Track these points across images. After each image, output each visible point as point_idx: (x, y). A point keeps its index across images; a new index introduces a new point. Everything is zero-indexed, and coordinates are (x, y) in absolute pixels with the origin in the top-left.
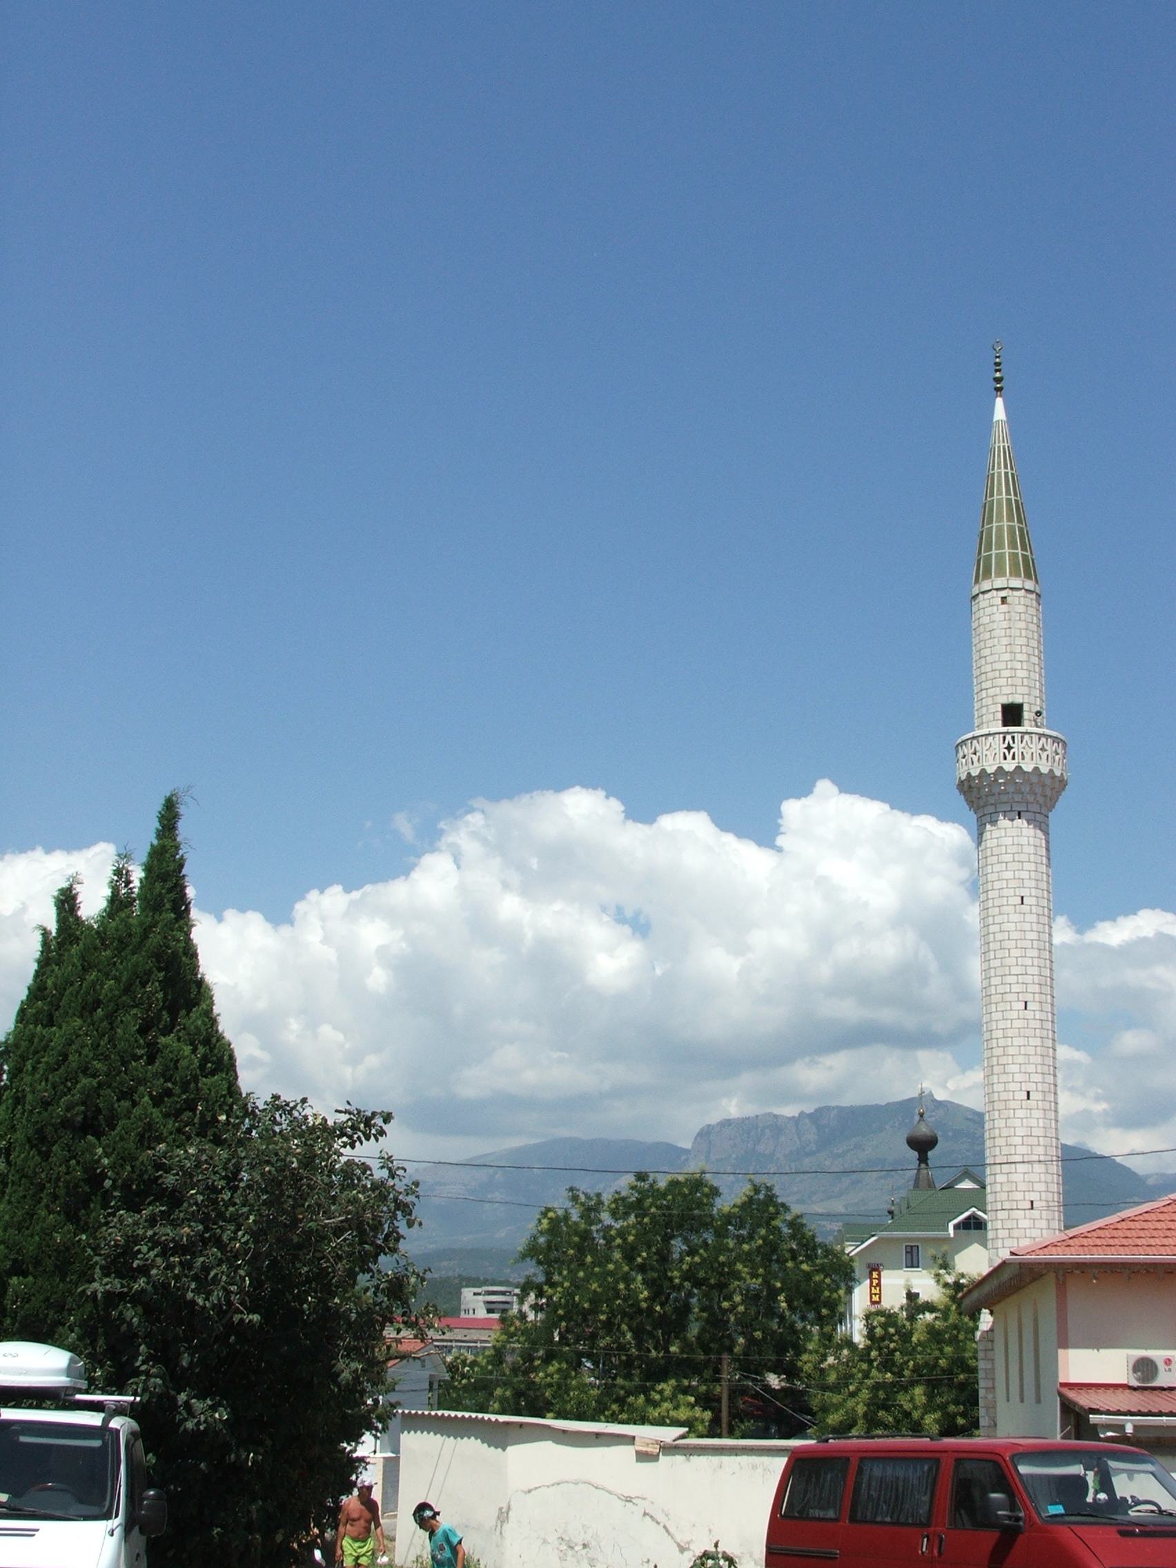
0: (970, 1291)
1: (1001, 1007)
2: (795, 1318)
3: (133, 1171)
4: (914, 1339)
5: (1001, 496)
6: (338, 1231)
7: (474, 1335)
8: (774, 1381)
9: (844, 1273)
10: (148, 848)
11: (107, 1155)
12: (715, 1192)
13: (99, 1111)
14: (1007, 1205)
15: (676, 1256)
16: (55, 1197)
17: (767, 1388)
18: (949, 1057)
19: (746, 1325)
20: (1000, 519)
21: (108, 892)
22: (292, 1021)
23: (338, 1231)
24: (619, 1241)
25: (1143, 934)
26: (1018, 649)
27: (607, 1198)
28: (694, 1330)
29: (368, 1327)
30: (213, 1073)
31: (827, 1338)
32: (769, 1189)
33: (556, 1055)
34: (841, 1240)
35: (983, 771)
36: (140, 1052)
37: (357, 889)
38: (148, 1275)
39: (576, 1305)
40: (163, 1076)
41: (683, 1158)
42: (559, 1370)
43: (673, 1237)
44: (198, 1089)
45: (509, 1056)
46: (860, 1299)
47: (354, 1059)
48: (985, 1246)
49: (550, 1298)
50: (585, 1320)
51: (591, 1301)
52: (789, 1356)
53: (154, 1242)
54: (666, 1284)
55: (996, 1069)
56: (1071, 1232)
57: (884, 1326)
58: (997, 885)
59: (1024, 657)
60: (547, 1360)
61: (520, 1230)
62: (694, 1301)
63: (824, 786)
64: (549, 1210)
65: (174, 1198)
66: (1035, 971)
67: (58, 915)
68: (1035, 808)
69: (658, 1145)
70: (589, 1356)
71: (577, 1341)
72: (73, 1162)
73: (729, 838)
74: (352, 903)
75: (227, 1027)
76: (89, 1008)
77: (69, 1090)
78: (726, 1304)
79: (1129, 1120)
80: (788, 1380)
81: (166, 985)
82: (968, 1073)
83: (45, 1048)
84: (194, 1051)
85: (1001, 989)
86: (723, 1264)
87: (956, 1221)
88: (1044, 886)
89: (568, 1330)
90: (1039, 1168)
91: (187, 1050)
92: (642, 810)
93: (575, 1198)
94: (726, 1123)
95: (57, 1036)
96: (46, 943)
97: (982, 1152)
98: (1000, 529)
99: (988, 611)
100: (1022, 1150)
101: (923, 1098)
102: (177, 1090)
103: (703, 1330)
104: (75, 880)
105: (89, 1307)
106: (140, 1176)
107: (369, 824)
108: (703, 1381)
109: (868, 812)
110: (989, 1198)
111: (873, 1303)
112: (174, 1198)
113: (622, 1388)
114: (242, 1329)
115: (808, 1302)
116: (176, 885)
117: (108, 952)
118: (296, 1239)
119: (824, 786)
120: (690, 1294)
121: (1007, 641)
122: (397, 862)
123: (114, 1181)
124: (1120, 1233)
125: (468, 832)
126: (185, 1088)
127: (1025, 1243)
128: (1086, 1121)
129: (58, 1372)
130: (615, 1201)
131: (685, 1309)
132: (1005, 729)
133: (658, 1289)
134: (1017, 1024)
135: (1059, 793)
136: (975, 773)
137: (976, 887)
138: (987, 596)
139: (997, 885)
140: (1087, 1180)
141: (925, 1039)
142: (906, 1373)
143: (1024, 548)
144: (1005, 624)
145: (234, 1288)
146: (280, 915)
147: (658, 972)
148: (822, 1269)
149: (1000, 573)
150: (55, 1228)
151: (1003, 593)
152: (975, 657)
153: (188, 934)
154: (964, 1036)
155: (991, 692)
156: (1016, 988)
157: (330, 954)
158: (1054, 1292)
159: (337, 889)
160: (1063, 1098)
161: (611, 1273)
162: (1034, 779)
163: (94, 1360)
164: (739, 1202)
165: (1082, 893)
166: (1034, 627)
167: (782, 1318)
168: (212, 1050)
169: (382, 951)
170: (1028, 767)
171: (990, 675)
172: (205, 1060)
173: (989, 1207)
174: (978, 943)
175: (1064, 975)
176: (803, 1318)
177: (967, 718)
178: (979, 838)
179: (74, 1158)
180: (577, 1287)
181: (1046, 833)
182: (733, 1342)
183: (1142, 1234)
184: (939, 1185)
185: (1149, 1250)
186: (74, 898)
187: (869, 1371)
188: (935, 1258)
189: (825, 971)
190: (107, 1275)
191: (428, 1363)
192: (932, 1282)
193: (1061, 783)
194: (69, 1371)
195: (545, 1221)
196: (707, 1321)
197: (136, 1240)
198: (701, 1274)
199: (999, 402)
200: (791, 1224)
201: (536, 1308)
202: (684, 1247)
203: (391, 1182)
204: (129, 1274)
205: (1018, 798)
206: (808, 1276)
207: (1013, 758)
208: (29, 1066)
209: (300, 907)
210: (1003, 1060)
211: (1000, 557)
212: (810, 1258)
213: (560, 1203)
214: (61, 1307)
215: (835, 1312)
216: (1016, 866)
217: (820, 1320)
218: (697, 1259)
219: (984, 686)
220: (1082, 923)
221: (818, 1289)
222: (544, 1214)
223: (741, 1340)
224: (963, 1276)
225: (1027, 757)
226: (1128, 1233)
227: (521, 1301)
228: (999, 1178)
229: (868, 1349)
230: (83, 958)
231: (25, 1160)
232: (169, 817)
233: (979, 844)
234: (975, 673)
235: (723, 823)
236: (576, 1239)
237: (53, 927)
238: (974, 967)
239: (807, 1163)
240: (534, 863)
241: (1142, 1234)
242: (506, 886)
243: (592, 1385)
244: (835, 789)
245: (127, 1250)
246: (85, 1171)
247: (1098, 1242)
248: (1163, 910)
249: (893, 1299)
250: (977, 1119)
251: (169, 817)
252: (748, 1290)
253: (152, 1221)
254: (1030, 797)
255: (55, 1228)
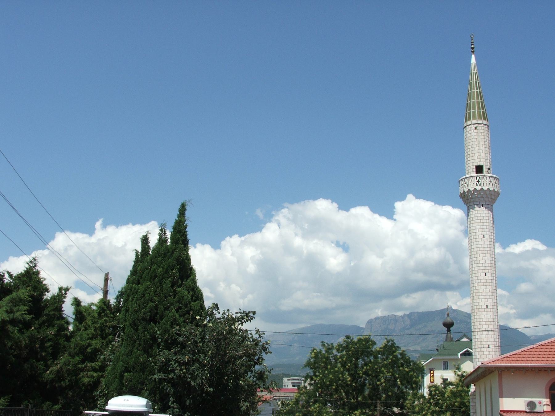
0: (467, 377)
1: (477, 275)
2: (403, 387)
3: (169, 336)
4: (446, 395)
5: (474, 90)
6: (241, 357)
7: (288, 394)
8: (396, 410)
9: (421, 371)
10: (174, 221)
11: (159, 330)
12: (374, 343)
13: (157, 313)
14: (480, 346)
15: (360, 366)
16: (140, 345)
17: (394, 413)
18: (458, 294)
19: (386, 390)
20: (474, 99)
21: (158, 237)
22: (221, 283)
23: (241, 357)
24: (340, 360)
25: (527, 249)
26: (481, 146)
27: (335, 345)
28: (367, 392)
29: (251, 392)
30: (195, 301)
31: (415, 395)
32: (393, 341)
33: (315, 294)
34: (419, 359)
35: (469, 190)
36: (171, 294)
37: (243, 236)
38: (174, 373)
39: (325, 383)
40: (179, 302)
41: (362, 331)
42: (318, 407)
43: (359, 359)
44: (190, 306)
45: (299, 295)
46: (427, 381)
47: (243, 296)
48: (472, 362)
49: (315, 381)
50: (328, 388)
51: (330, 382)
52: (401, 401)
53: (176, 361)
54: (357, 375)
55: (475, 298)
56: (503, 356)
57: (435, 391)
58: (475, 231)
59: (483, 149)
60: (315, 402)
61: (304, 357)
62: (367, 381)
63: (410, 197)
64: (314, 349)
65: (183, 346)
66: (489, 262)
67: (142, 245)
68: (487, 203)
69: (353, 326)
70: (330, 402)
71: (325, 396)
72: (146, 332)
73: (376, 216)
74: (242, 242)
75: (200, 284)
76: (153, 277)
77: (145, 307)
78: (378, 383)
79: (524, 316)
80: (401, 410)
81: (180, 270)
82: (464, 299)
83: (136, 293)
84: (189, 293)
85: (476, 268)
86: (377, 369)
87: (461, 353)
88: (492, 231)
89: (322, 392)
90: (491, 333)
91: (186, 293)
92: (345, 206)
93: (324, 345)
94: (377, 318)
95: (141, 288)
96: (137, 255)
97: (471, 328)
98: (474, 102)
99: (470, 132)
100: (485, 326)
101: (449, 308)
102: (183, 307)
103: (370, 392)
104: (148, 233)
105: (153, 383)
106: (171, 337)
107: (247, 213)
108: (370, 410)
109: (426, 206)
110: (473, 344)
111: (431, 382)
112: (183, 346)
113: (342, 413)
114: (208, 393)
115: (408, 382)
116: (184, 234)
117: (160, 259)
118: (226, 360)
119: (410, 197)
120: (365, 379)
121: (477, 143)
122: (257, 226)
123: (162, 339)
124: (521, 356)
125: (284, 215)
126: (186, 307)
127: (486, 360)
128: (508, 316)
129: (142, 406)
130: (339, 346)
131: (364, 385)
132: (477, 175)
133: (354, 377)
134: (483, 281)
135: (497, 197)
136: (466, 190)
137: (467, 232)
138: (470, 127)
139: (475, 231)
140: (508, 338)
141: (449, 287)
142: (444, 407)
143: (483, 109)
144: (476, 137)
145: (204, 377)
146: (216, 246)
147: (352, 264)
148: (412, 370)
149: (474, 118)
150: (140, 356)
151: (475, 126)
152: (465, 149)
153: (187, 252)
154: (463, 286)
155: (472, 161)
156: (482, 268)
157: (234, 259)
158: (497, 377)
159: (237, 236)
160: (499, 308)
161: (337, 372)
162: (488, 193)
163: (154, 402)
164: (382, 346)
165: (505, 235)
166: (487, 138)
167: (399, 387)
168: (195, 292)
169: (252, 258)
170: (485, 188)
171: (471, 155)
172: (192, 296)
173: (473, 347)
174: (468, 252)
175: (499, 264)
176: (406, 388)
177: (463, 171)
178: (468, 214)
179: (147, 331)
180: (325, 377)
181: (492, 212)
182: (381, 396)
183: (529, 356)
184: (455, 340)
185: (542, 362)
186: (148, 239)
187: (430, 407)
188: (455, 365)
189: (412, 263)
190: (160, 373)
191: (272, 405)
192: (453, 375)
193: (498, 194)
194: (147, 406)
195: (313, 353)
196: (371, 389)
197: (169, 360)
198: (370, 373)
199: (473, 56)
200: (401, 354)
201: (310, 384)
202: (363, 363)
203: (259, 339)
204: (166, 372)
205: (482, 199)
206: (408, 372)
208: (131, 298)
209: (223, 243)
210: (478, 294)
211: (474, 112)
212: (408, 366)
213: (318, 346)
214: (143, 384)
215: (418, 385)
216: (481, 224)
217: (412, 388)
218: (368, 368)
219: (469, 159)
220: (504, 245)
221: (411, 377)
222: (313, 351)
223: (384, 395)
224: (464, 372)
225: (485, 184)
226: (524, 356)
227: (305, 382)
228: (477, 337)
229: (430, 399)
230: (151, 260)
231: (129, 332)
232: (182, 210)
233: (468, 216)
234: (466, 155)
235: (374, 210)
236: (324, 360)
237: (139, 249)
238: (466, 262)
239: (407, 332)
240: (306, 226)
241: (529, 356)
242: (296, 235)
243: (331, 412)
244: (414, 198)
245: (167, 363)
246: (151, 336)
247: (514, 359)
248: (521, 242)
249: (438, 382)
250: (469, 316)
251: (182, 210)
252: (386, 377)
253: (175, 353)
254: (487, 199)
255: (140, 356)
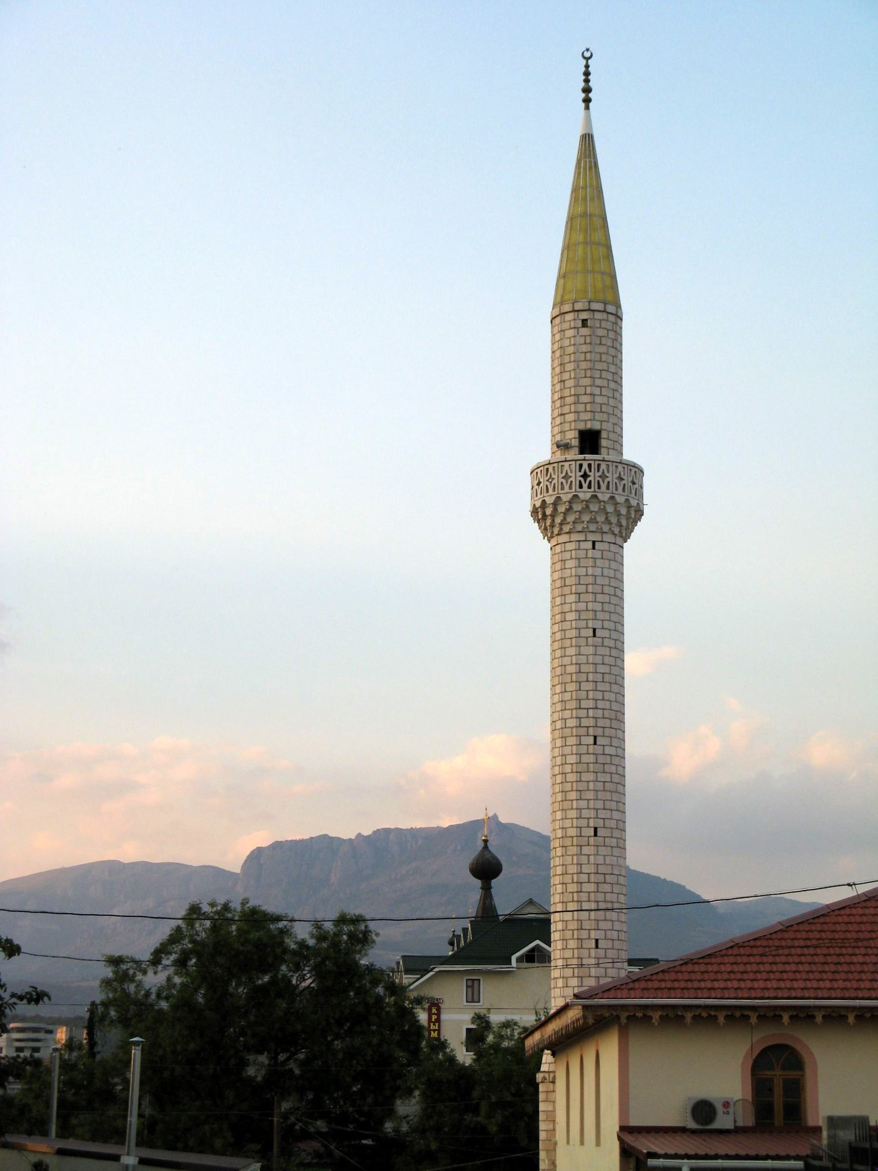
132: (582, 457)
135: (635, 523)
207: (608, 488)
